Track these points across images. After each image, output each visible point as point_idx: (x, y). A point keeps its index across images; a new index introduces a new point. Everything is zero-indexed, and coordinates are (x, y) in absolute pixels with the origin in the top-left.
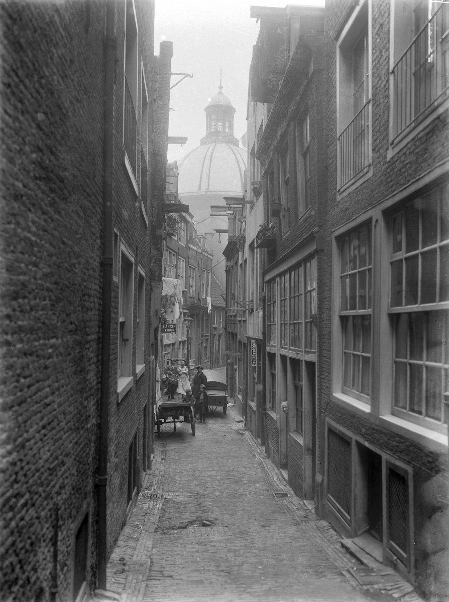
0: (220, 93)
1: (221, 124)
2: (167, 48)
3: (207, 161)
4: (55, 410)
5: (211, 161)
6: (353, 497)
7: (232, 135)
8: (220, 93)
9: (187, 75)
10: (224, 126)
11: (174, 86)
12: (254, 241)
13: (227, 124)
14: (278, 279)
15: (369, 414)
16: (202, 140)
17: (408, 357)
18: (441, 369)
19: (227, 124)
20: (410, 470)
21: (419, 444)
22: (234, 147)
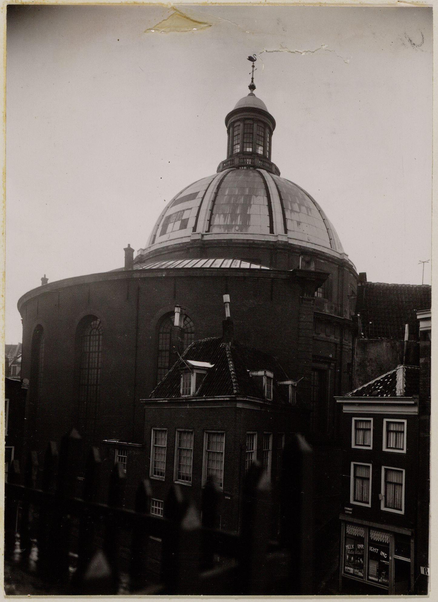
0: (252, 94)
8: (252, 94)
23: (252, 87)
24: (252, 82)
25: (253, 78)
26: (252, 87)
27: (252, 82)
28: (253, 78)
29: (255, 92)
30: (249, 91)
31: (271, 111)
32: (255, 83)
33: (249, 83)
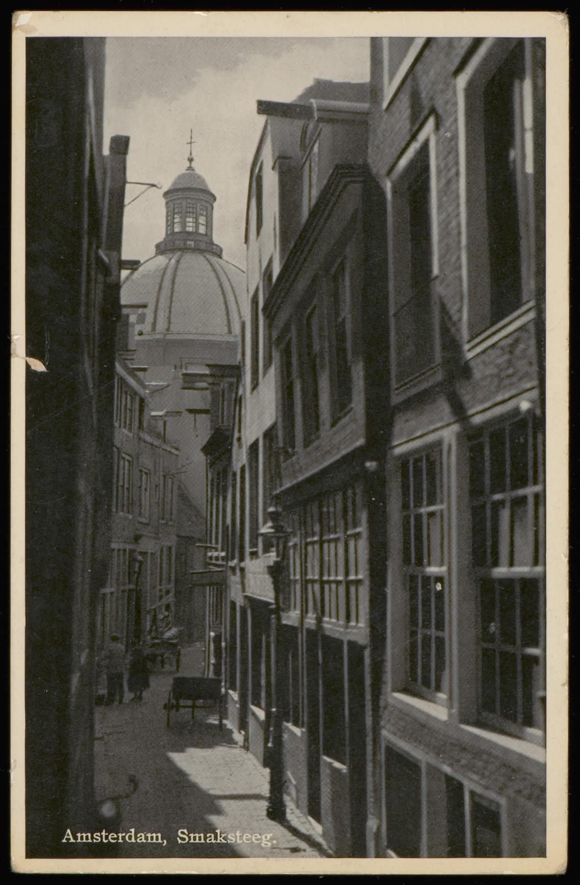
0: (190, 168)
1: (191, 220)
2: (121, 145)
3: (167, 284)
4: (334, 179)
5: (173, 282)
6: (301, 696)
7: (209, 235)
8: (190, 168)
9: (153, 185)
10: (197, 224)
11: (129, 203)
12: (257, 440)
13: (202, 220)
14: (489, 379)
15: (445, 722)
16: (158, 246)
17: (251, 550)
18: (257, 547)
19: (202, 220)
20: (503, 801)
21: (406, 650)
22: (214, 259)
23: (191, 160)
24: (191, 154)
26: (191, 160)
27: (191, 154)
29: (194, 164)
30: (187, 164)
31: (213, 191)
32: (194, 155)
33: (187, 155)
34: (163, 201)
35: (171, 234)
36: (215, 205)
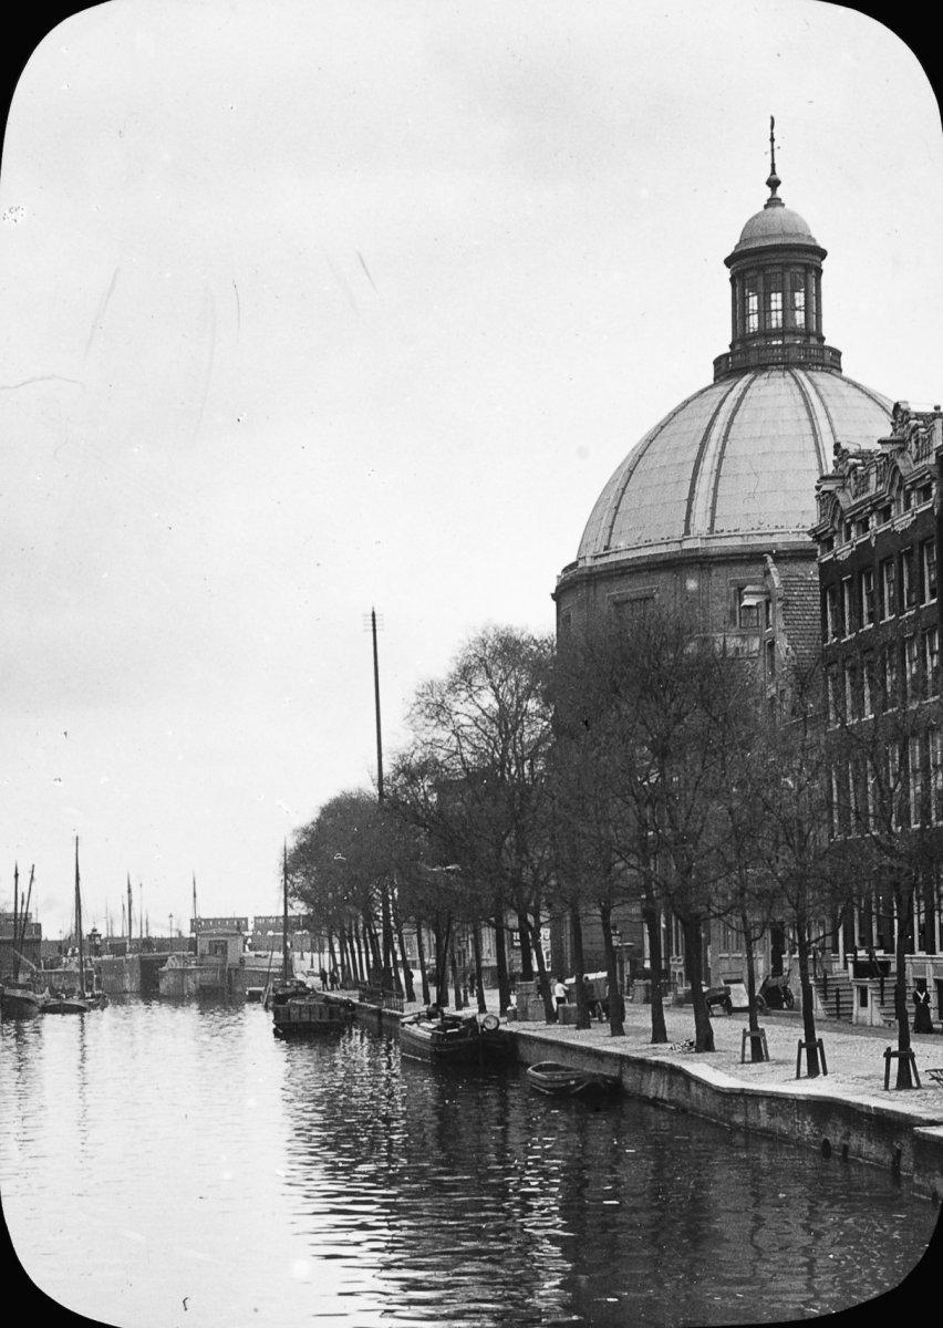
7: (813, 332)
8: (773, 202)
23: (773, 184)
24: (773, 172)
25: (773, 165)
26: (773, 184)
27: (773, 172)
28: (773, 165)
29: (780, 192)
30: (767, 192)
32: (780, 175)
34: (727, 273)
35: (741, 337)
36: (825, 265)
